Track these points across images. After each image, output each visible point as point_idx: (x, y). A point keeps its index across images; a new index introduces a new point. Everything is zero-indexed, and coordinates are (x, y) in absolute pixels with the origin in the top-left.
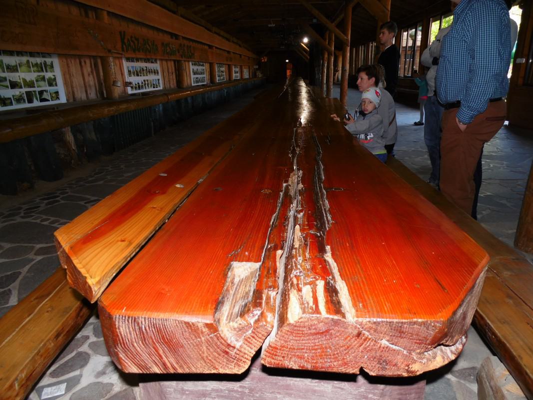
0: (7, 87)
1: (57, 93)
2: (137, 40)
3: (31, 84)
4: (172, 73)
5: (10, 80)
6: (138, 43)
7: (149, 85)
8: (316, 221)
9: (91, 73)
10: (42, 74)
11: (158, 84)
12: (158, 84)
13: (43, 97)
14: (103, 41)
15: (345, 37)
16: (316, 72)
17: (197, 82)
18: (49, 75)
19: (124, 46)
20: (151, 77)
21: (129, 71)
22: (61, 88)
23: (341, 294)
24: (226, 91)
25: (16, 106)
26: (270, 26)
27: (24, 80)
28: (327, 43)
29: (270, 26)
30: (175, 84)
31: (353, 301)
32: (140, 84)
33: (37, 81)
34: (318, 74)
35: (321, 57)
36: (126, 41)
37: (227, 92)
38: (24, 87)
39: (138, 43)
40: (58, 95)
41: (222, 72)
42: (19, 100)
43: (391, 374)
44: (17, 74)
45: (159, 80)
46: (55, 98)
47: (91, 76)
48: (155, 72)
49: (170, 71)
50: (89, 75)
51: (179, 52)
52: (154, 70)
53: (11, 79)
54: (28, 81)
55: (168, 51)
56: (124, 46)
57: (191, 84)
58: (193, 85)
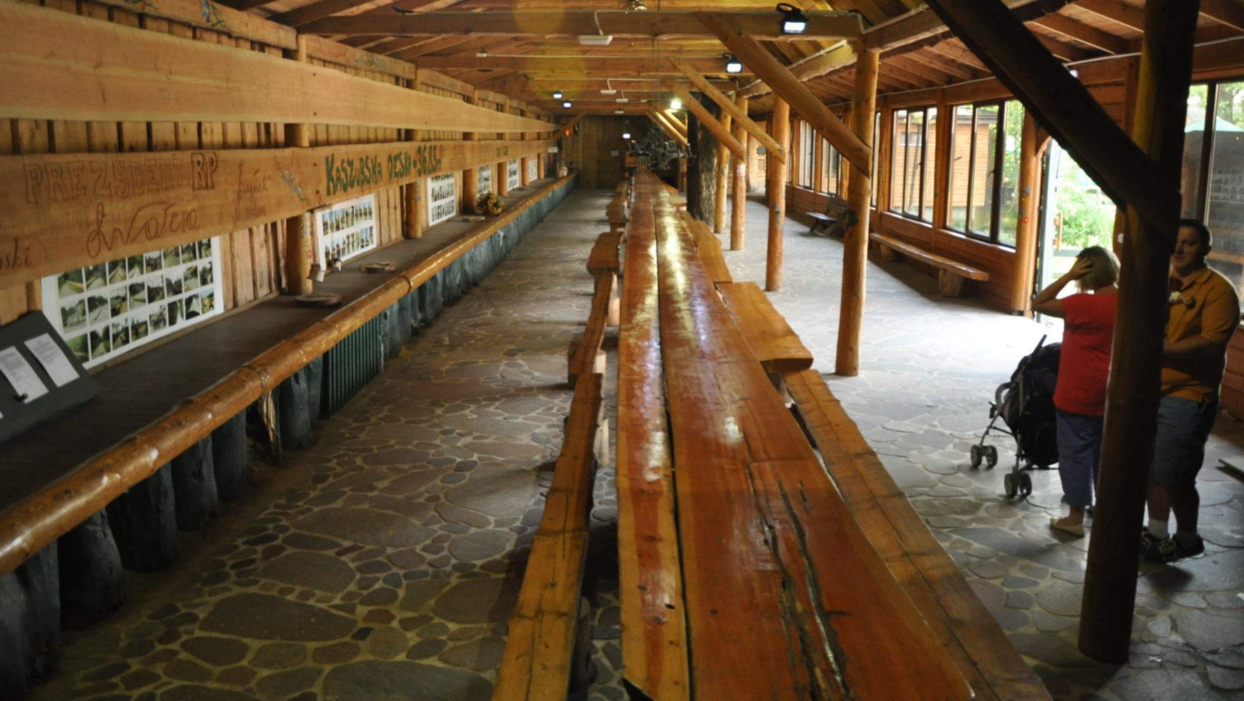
0: (143, 301)
1: (211, 296)
2: (350, 163)
3: (175, 288)
4: (395, 208)
5: (149, 288)
6: (352, 170)
7: (355, 245)
8: (569, 173)
9: (264, 244)
10: (192, 264)
11: (369, 238)
12: (369, 238)
13: (191, 310)
14: (301, 186)
15: (777, 146)
16: (704, 184)
17: (439, 215)
18: (201, 264)
19: (331, 185)
20: (363, 225)
21: (325, 224)
22: (218, 287)
23: (236, 30)
24: (502, 234)
25: (153, 335)
26: (603, 92)
27: (169, 282)
28: (728, 128)
29: (603, 92)
30: (400, 232)
31: (689, 11)
32: (341, 246)
33: (186, 279)
34: (708, 187)
35: (715, 151)
36: (334, 173)
37: (505, 237)
38: (168, 292)
39: (352, 170)
40: (213, 300)
41: (487, 179)
42: (157, 323)
43: (498, 223)
44: (158, 273)
45: (371, 228)
46: (208, 307)
47: (264, 249)
48: (365, 214)
49: (392, 204)
50: (262, 246)
51: (415, 166)
52: (365, 209)
53: (151, 286)
54: (173, 282)
55: (397, 170)
56: (331, 185)
57: (428, 224)
58: (431, 224)
